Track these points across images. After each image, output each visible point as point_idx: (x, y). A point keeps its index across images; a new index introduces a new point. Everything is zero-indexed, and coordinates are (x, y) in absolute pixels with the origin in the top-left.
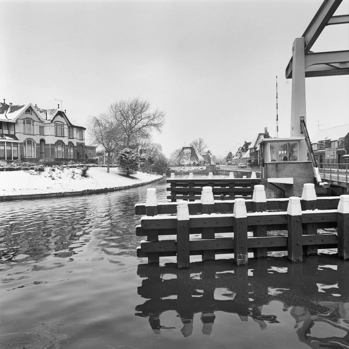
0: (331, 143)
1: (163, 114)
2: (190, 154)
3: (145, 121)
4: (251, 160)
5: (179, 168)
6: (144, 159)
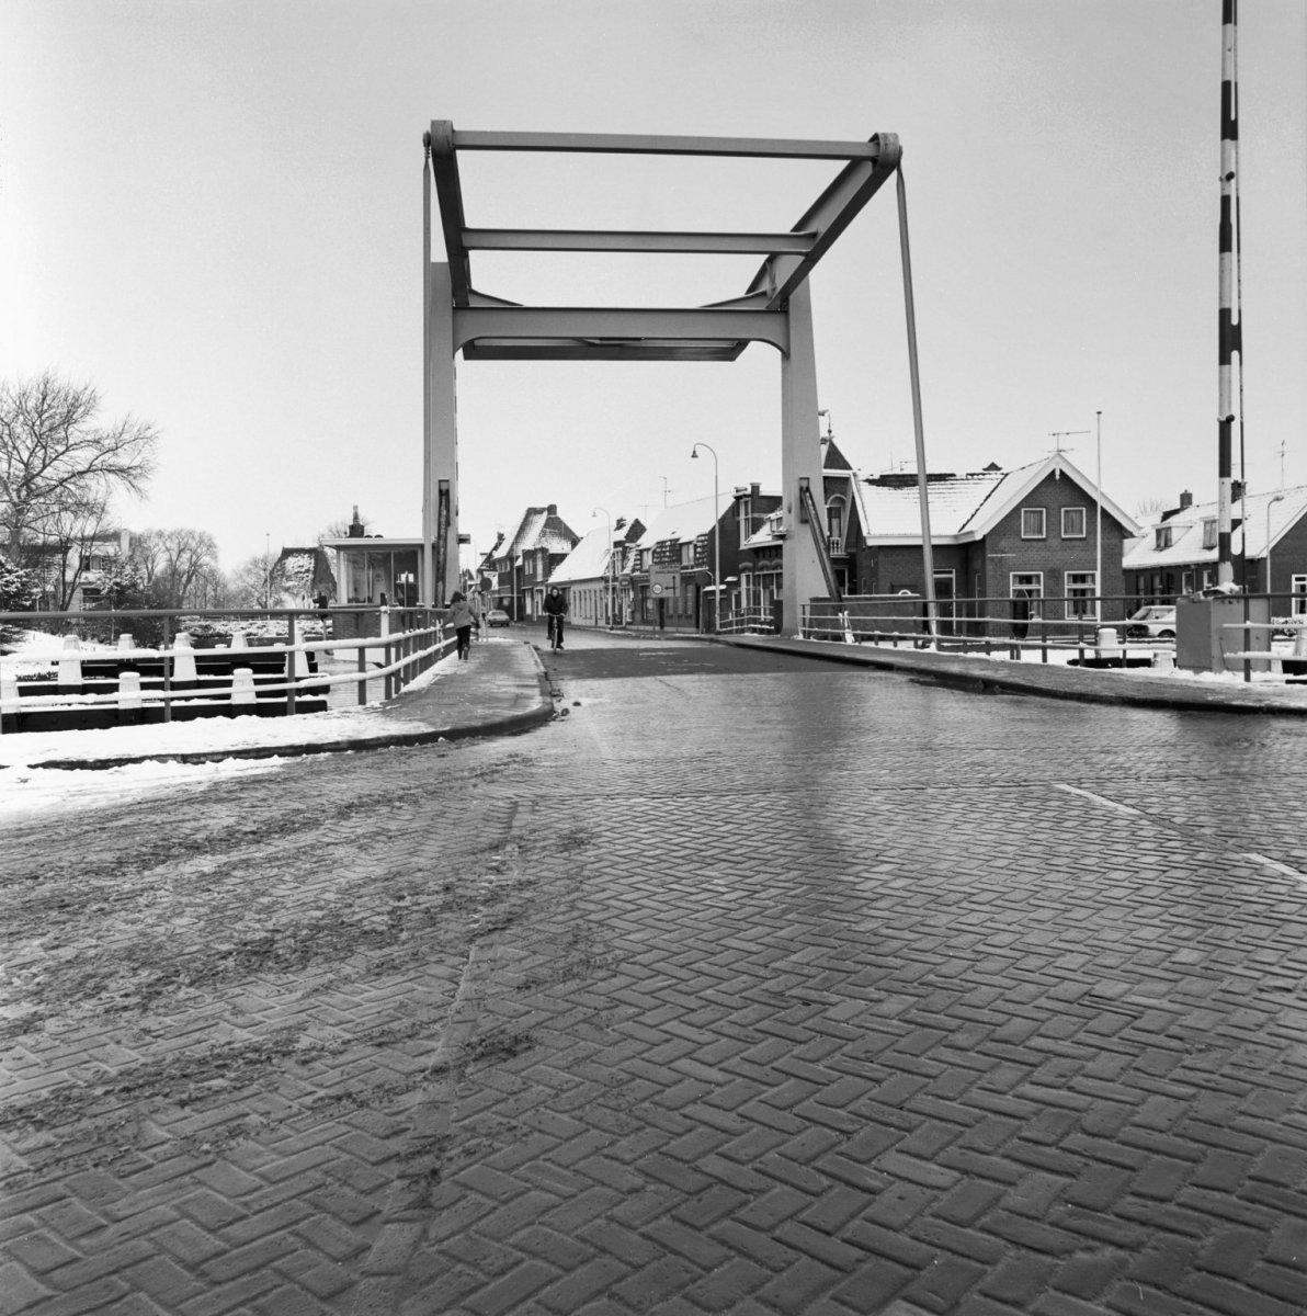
0: (680, 550)
1: (149, 433)
2: (311, 576)
3: (82, 458)
4: (501, 599)
5: (244, 624)
6: (97, 591)
